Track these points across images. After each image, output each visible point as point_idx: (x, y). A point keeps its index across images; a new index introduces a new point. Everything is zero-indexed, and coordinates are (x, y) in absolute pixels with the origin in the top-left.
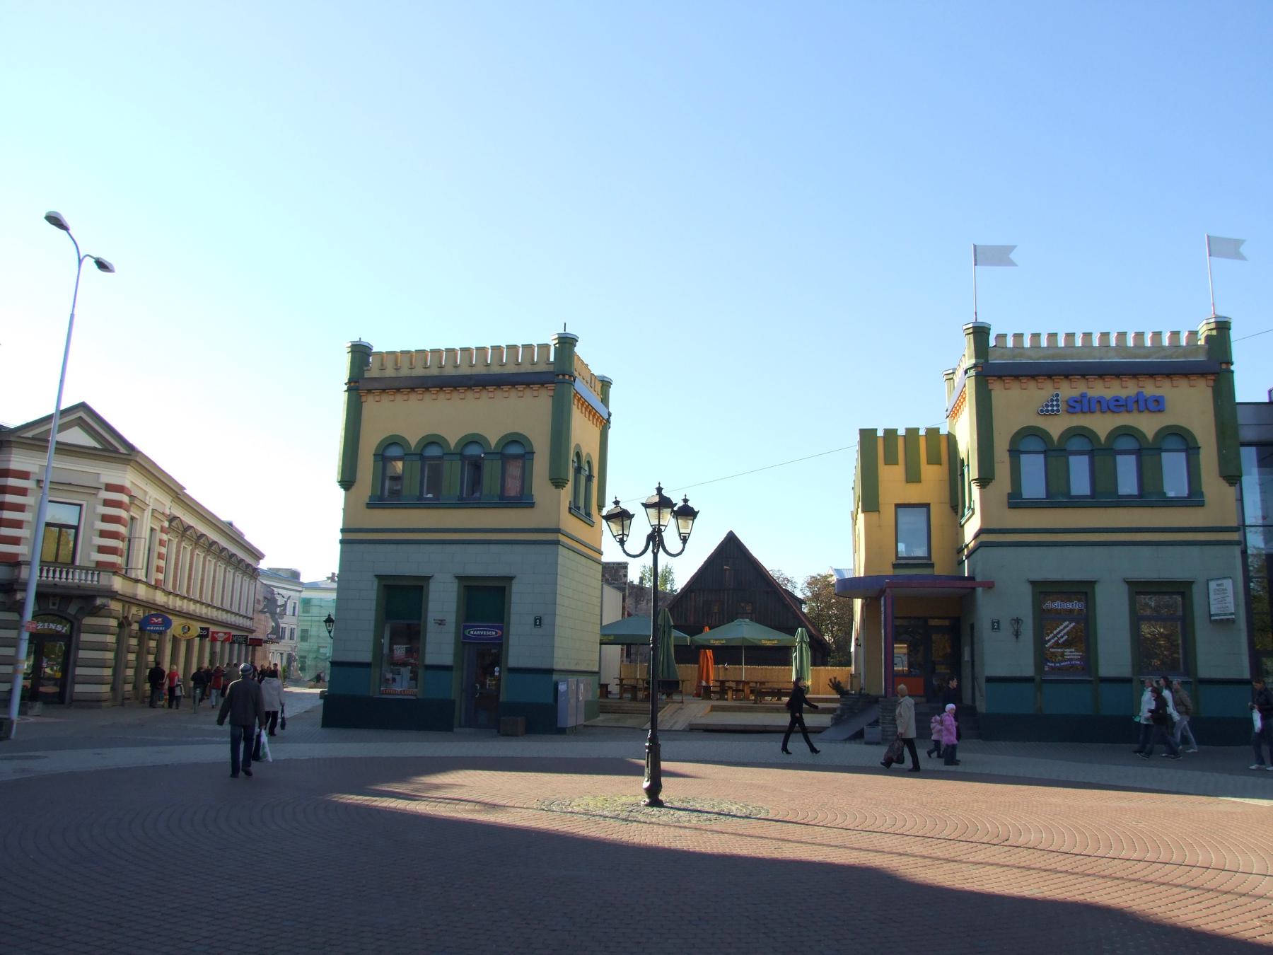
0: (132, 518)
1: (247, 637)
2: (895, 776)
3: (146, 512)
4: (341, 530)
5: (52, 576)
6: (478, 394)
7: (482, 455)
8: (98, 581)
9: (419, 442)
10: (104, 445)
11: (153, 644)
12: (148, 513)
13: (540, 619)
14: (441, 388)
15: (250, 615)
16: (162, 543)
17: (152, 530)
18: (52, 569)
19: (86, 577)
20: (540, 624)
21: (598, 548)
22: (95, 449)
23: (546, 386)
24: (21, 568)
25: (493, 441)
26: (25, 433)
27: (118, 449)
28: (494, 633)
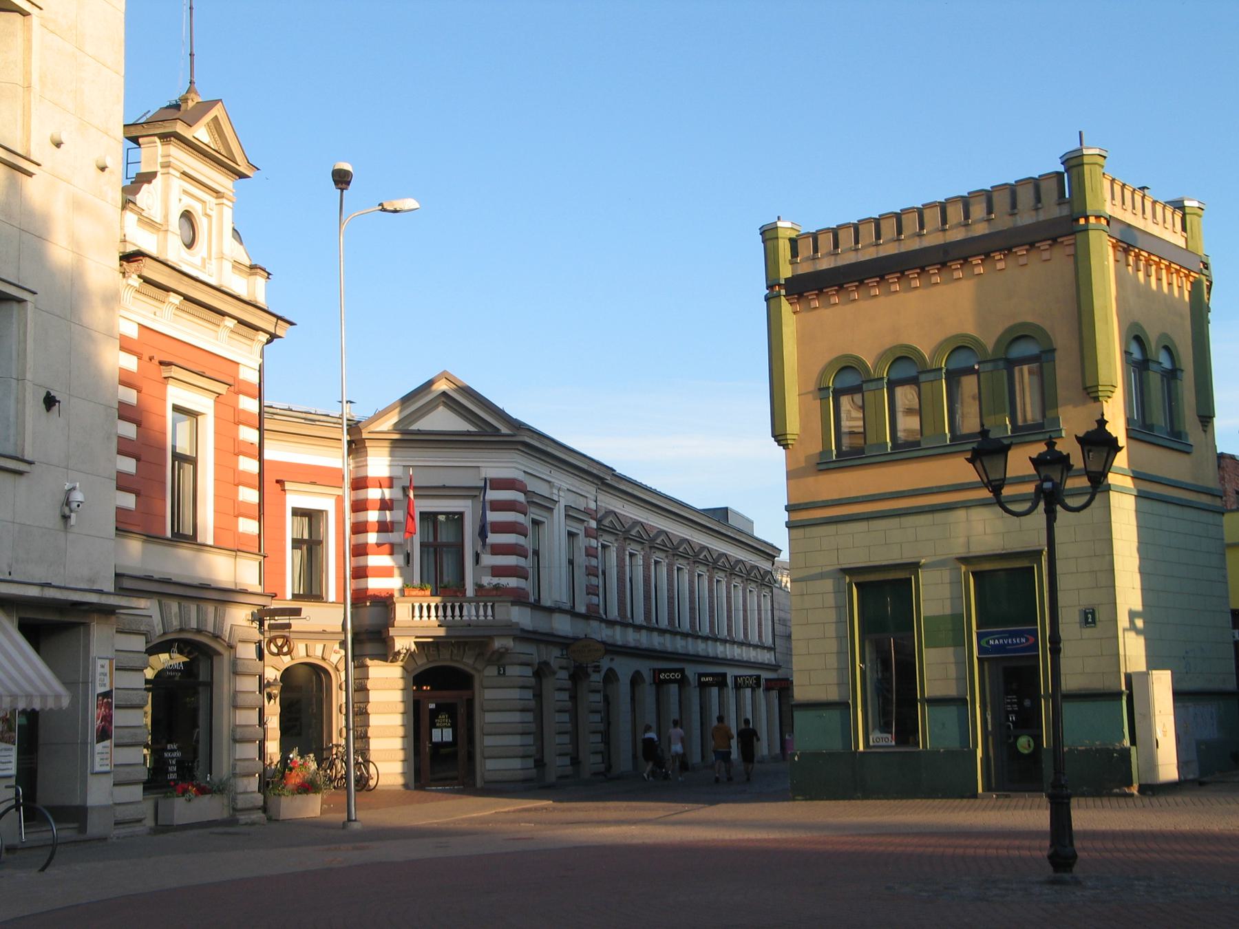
0: (536, 523)
1: (758, 677)
2: (734, 801)
3: (556, 512)
4: (786, 506)
5: (483, 614)
6: (1025, 257)
7: (976, 367)
8: (493, 615)
9: (998, 342)
10: (480, 427)
11: (356, 709)
12: (559, 512)
13: (1093, 614)
14: (1032, 245)
15: (768, 641)
16: (590, 553)
17: (571, 535)
18: (457, 605)
19: (477, 611)
20: (1094, 621)
21: (750, 532)
22: (468, 433)
23: (1059, 240)
24: (88, 634)
25: (989, 343)
26: (380, 424)
27: (498, 430)
28: (1023, 640)
